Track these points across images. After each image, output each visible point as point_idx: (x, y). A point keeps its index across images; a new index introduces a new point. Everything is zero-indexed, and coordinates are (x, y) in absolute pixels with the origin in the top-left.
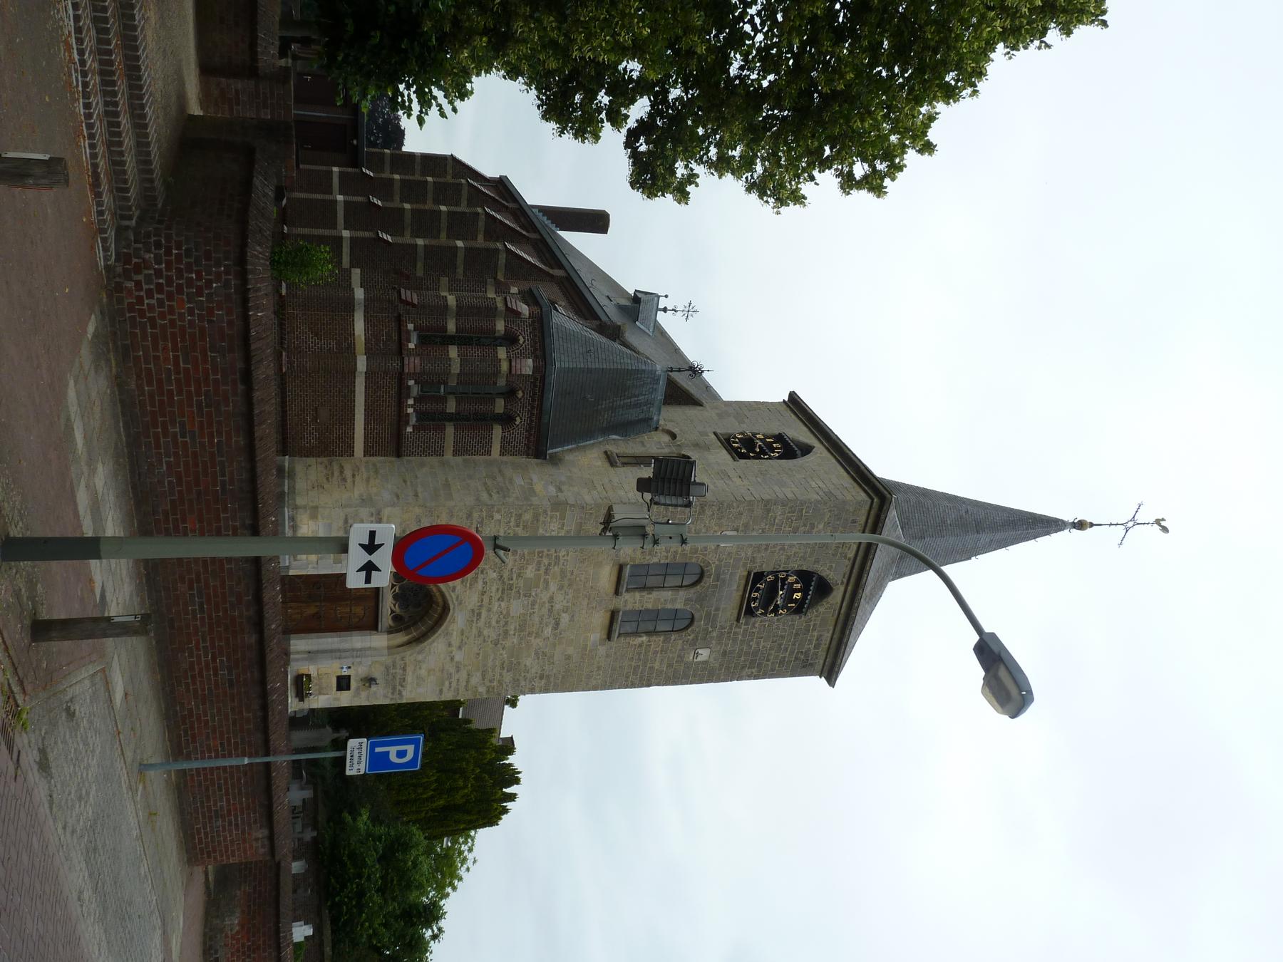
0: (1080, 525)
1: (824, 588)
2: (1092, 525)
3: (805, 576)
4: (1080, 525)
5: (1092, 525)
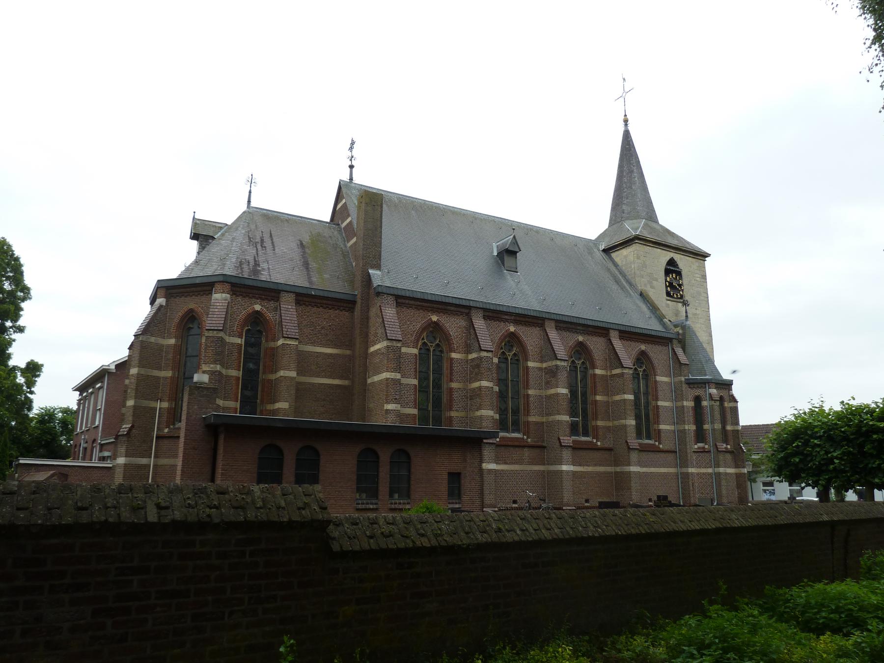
0: (626, 121)
1: (672, 262)
2: (625, 115)
3: (667, 272)
4: (626, 121)
5: (625, 115)
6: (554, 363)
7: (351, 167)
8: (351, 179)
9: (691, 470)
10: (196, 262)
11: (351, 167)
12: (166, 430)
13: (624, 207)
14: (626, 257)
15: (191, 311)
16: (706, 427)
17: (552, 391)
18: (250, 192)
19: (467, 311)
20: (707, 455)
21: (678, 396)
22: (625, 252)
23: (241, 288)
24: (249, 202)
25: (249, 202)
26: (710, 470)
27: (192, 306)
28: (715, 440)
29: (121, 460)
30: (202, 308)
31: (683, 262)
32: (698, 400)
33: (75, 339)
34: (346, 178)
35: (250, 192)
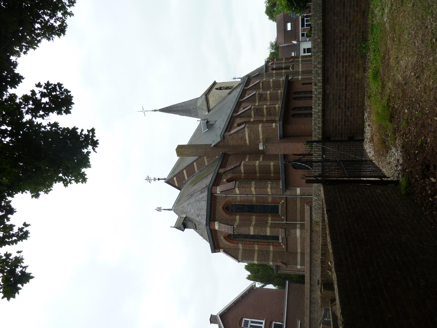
0: (155, 111)
4: (155, 111)
6: (257, 95)
7: (159, 179)
8: (165, 179)
9: (300, 70)
10: (196, 228)
11: (159, 179)
12: (284, 247)
13: (191, 108)
14: (213, 101)
15: (223, 207)
16: (283, 66)
17: (268, 96)
18: (164, 210)
19: (233, 118)
20: (294, 66)
21: (271, 75)
22: (211, 102)
23: (211, 217)
24: (169, 210)
25: (169, 210)
26: (300, 65)
27: (221, 207)
28: (288, 63)
29: (300, 77)
30: (222, 201)
31: (216, 86)
32: (273, 69)
33: (231, 278)
34: (164, 181)
35: (164, 210)
